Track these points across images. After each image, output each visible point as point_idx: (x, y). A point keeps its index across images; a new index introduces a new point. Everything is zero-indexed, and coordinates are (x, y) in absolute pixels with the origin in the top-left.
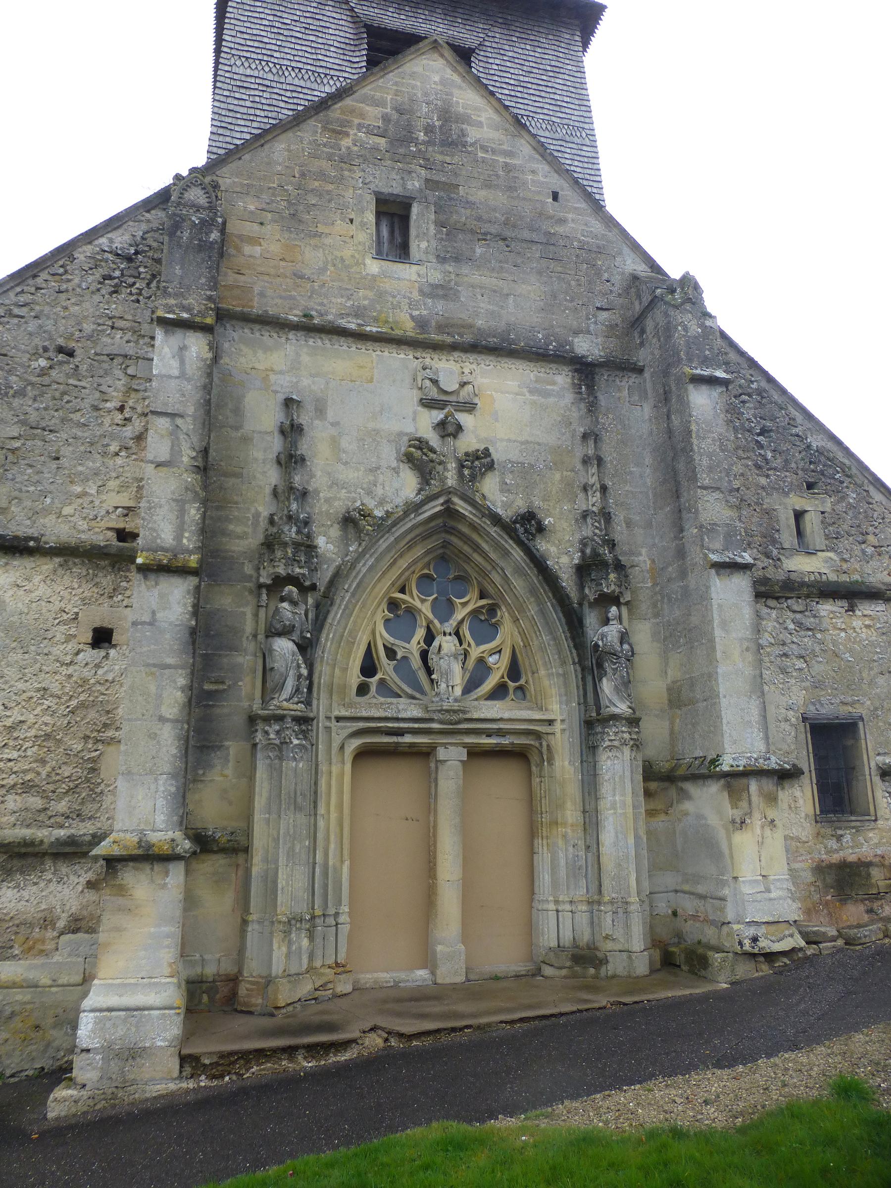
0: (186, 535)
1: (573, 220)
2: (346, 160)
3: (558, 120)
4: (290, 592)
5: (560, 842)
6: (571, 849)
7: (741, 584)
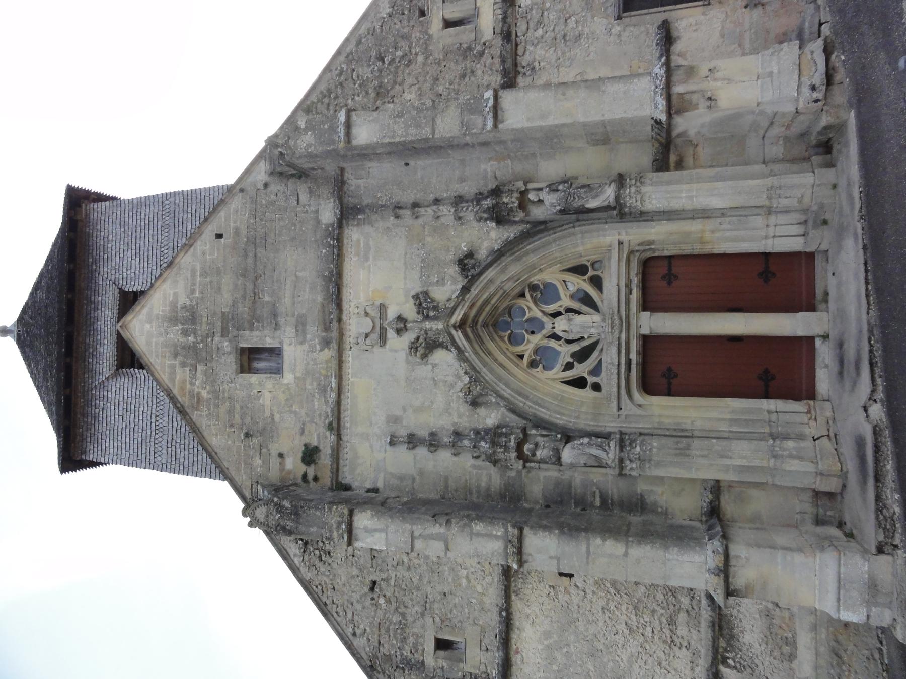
0: (494, 533)
1: (235, 223)
2: (216, 394)
3: (160, 223)
4: (528, 450)
5: (717, 235)
6: (723, 227)
7: (508, 98)
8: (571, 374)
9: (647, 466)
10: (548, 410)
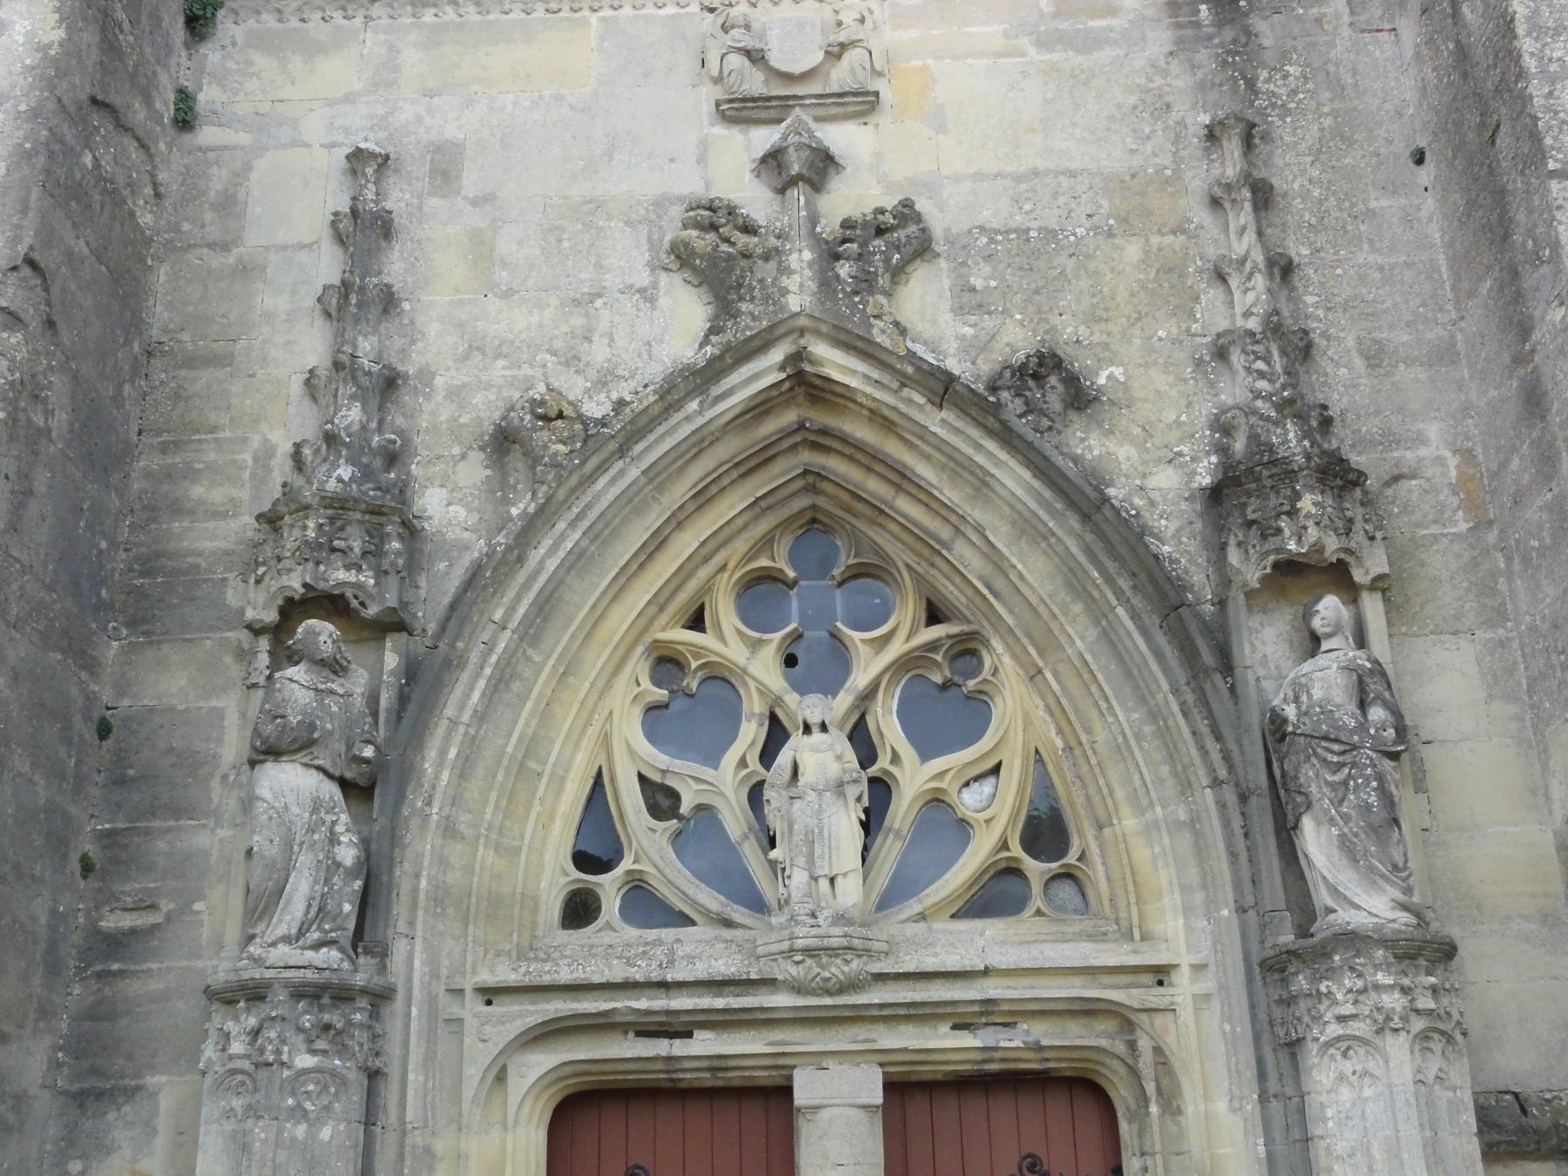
8: (630, 800)
9: (238, 1103)
10: (481, 717)
